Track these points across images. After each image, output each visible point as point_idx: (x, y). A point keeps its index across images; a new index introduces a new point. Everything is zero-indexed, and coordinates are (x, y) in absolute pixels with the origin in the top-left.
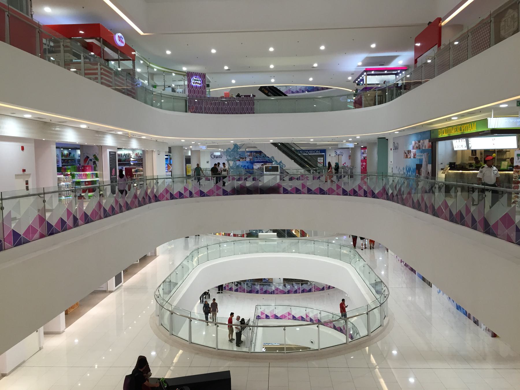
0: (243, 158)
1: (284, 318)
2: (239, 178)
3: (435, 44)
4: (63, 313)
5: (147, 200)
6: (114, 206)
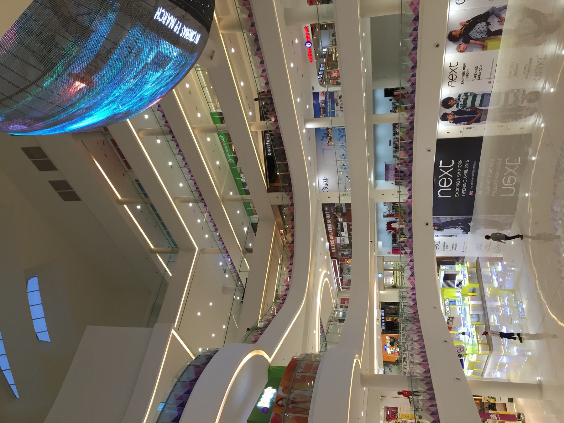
0: (328, 132)
1: (415, 59)
2: (410, 238)
3: (26, 288)
4: (49, 340)
5: (416, 317)
6: (421, 356)
